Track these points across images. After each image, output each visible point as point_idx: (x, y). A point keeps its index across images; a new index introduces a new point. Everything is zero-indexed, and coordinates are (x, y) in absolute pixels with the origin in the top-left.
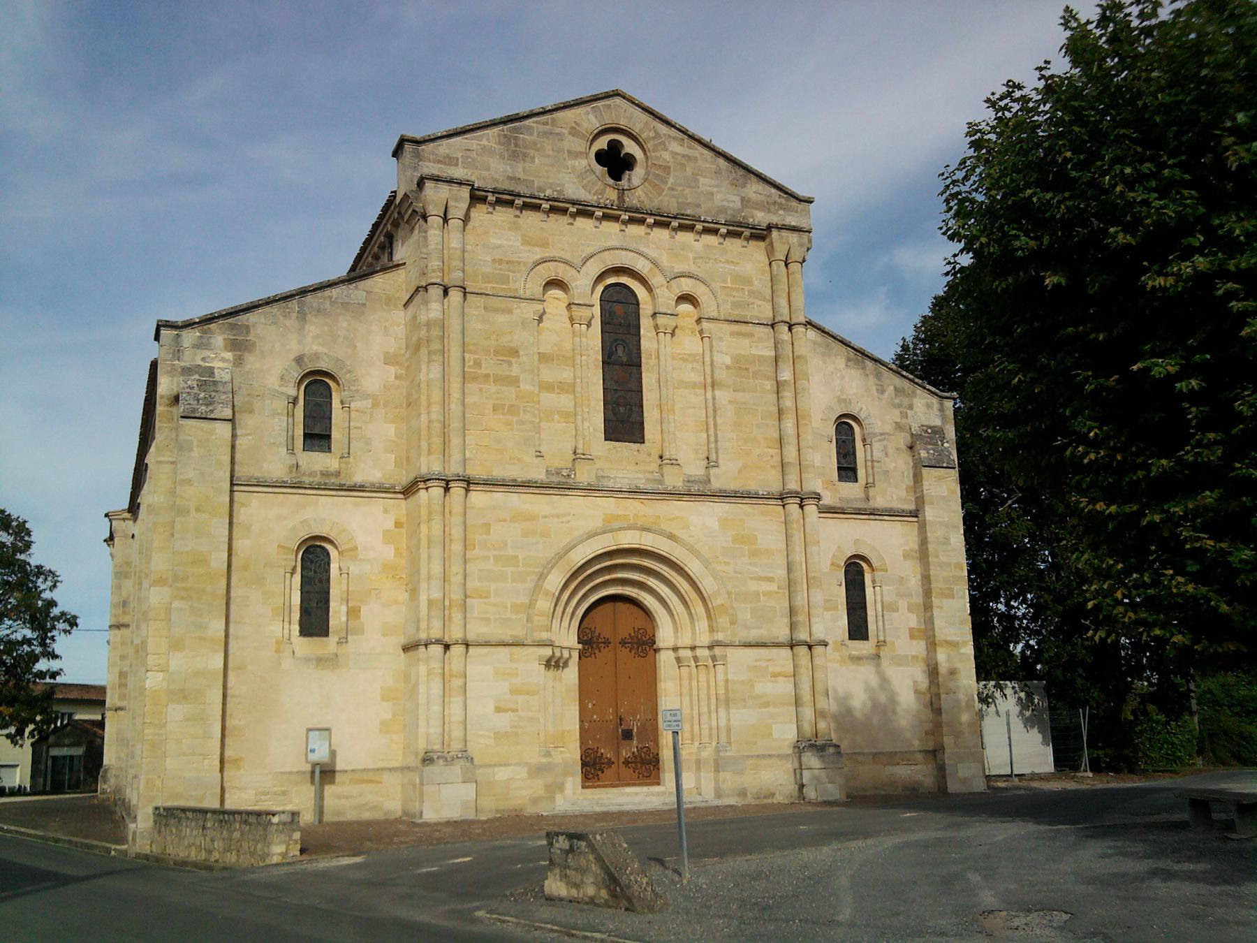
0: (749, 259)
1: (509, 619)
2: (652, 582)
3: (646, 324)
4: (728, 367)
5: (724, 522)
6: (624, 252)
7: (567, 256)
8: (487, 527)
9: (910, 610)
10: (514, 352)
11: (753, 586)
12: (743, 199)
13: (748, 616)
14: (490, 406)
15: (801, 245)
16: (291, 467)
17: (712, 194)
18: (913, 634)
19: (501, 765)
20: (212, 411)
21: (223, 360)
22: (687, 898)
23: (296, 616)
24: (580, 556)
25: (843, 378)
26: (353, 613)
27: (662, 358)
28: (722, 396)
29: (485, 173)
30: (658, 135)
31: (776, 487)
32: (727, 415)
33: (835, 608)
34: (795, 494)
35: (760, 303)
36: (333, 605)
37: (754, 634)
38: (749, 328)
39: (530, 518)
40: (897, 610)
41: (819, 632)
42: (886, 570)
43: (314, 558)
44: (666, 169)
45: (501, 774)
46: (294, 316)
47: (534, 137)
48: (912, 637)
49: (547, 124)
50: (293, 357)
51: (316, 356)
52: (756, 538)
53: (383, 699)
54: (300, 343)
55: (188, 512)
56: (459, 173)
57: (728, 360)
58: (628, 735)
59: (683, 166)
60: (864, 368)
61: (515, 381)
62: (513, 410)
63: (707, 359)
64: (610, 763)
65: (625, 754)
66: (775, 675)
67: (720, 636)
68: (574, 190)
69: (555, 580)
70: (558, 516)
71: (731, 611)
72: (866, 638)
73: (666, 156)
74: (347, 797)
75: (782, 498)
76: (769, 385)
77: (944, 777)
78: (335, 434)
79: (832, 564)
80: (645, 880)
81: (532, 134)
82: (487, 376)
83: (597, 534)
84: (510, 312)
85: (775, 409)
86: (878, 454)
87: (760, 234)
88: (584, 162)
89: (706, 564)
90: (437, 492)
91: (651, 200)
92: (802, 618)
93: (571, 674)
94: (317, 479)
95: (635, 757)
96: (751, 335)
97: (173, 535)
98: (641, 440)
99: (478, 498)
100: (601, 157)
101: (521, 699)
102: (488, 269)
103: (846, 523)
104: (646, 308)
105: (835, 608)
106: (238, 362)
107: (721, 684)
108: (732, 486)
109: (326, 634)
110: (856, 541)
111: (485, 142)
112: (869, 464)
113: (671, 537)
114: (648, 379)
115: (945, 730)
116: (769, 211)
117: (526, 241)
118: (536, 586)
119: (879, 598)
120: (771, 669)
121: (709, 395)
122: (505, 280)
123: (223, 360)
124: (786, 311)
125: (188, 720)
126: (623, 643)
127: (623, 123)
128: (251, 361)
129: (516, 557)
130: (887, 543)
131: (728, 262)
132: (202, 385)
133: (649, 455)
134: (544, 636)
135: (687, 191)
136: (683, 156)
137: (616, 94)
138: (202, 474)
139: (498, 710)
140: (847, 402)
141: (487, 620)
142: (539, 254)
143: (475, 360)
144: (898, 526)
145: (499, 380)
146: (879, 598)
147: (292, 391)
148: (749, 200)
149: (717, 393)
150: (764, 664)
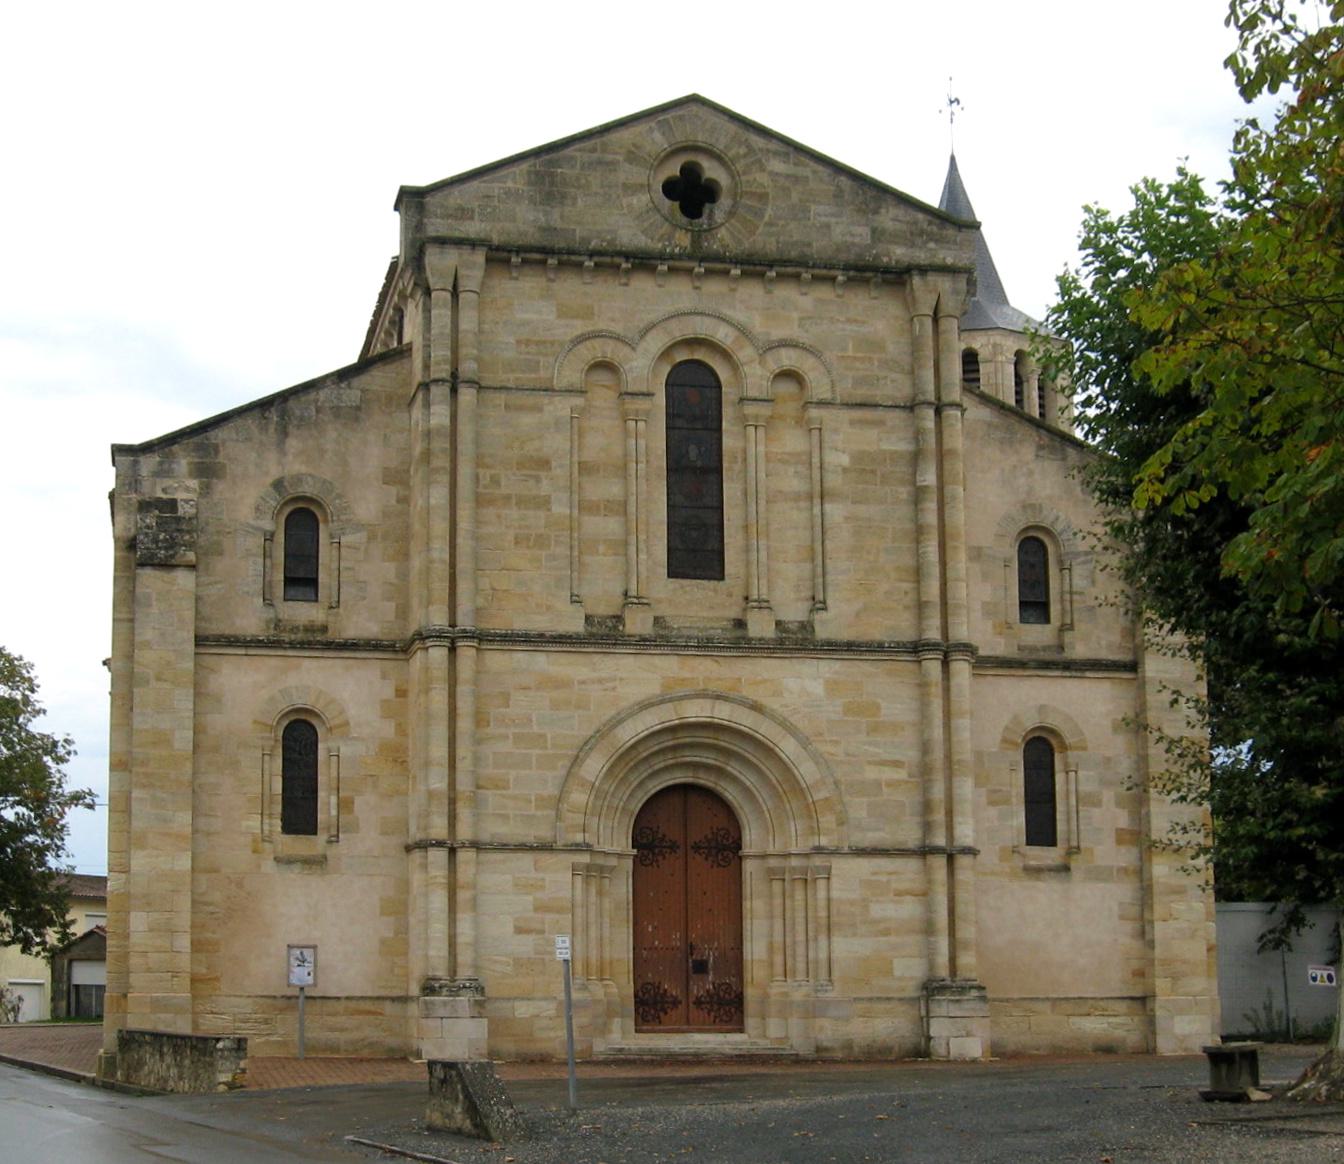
0: (873, 320)
1: (534, 816)
2: (733, 768)
3: (728, 413)
4: (845, 470)
5: (832, 687)
6: (698, 319)
7: (618, 328)
8: (506, 698)
9: (1118, 804)
10: (544, 464)
11: (871, 773)
12: (874, 231)
13: (864, 814)
14: (510, 537)
15: (956, 292)
16: (268, 622)
17: (828, 226)
18: (1121, 837)
19: (523, 999)
20: (172, 556)
21: (187, 489)
22: (266, 1068)
23: (278, 808)
24: (630, 732)
25: (1031, 473)
26: (345, 805)
27: (751, 461)
28: (835, 511)
29: (509, 226)
30: (750, 149)
31: (908, 635)
32: (840, 539)
33: (1007, 801)
34: (932, 647)
35: (894, 376)
36: (322, 794)
37: (871, 838)
38: (878, 414)
39: (560, 684)
40: (1098, 804)
41: (965, 834)
42: (1084, 749)
43: (299, 739)
44: (763, 197)
45: (523, 1010)
46: (272, 429)
47: (577, 171)
48: (1120, 841)
49: (594, 150)
50: (270, 480)
51: (298, 479)
52: (878, 708)
53: (382, 914)
54: (280, 463)
55: (148, 682)
56: (473, 228)
57: (845, 460)
58: (701, 967)
59: (786, 191)
60: (1064, 459)
61: (544, 503)
62: (541, 541)
63: (816, 460)
64: (676, 1003)
65: (696, 990)
66: (899, 894)
67: (824, 841)
68: (631, 236)
69: (595, 766)
70: (600, 681)
71: (839, 808)
72: (1053, 843)
73: (763, 178)
74: (342, 1030)
75: (917, 649)
76: (904, 492)
77: (1154, 1033)
78: (322, 578)
79: (1005, 740)
80: (509, 1112)
81: (573, 167)
82: (508, 498)
83: (652, 705)
84: (540, 410)
85: (909, 526)
86: (1079, 582)
87: (896, 277)
88: (645, 198)
89: (804, 742)
90: (438, 654)
91: (739, 242)
92: (939, 816)
93: (622, 888)
94: (300, 636)
95: (711, 997)
96: (881, 423)
97: (131, 709)
98: (720, 576)
99: (498, 660)
100: (670, 189)
101: (549, 917)
102: (510, 354)
103: (1086, 684)
104: (729, 393)
105: (1007, 801)
106: (206, 490)
107: (822, 903)
108: (845, 635)
109: (314, 832)
110: (1042, 709)
111: (510, 184)
112: (1067, 597)
113: (756, 707)
114: (731, 490)
115: (1158, 969)
116: (913, 245)
117: (561, 315)
118: (569, 773)
119: (1072, 788)
120: (894, 885)
121: (817, 510)
122: (534, 367)
123: (187, 489)
124: (931, 387)
125: (151, 930)
126: (697, 848)
127: (701, 138)
128: (220, 487)
129: (542, 736)
130: (1087, 708)
131: (849, 321)
132: (162, 524)
133: (730, 595)
134: (579, 838)
135: (792, 225)
136: (788, 176)
137: (695, 100)
138: (162, 635)
139: (519, 930)
140: (1035, 508)
141: (505, 817)
142: (579, 327)
143: (492, 477)
144: (1106, 686)
145: (522, 502)
146: (1072, 788)
147: (267, 524)
148: (883, 232)
149: (828, 507)
150: (884, 878)
